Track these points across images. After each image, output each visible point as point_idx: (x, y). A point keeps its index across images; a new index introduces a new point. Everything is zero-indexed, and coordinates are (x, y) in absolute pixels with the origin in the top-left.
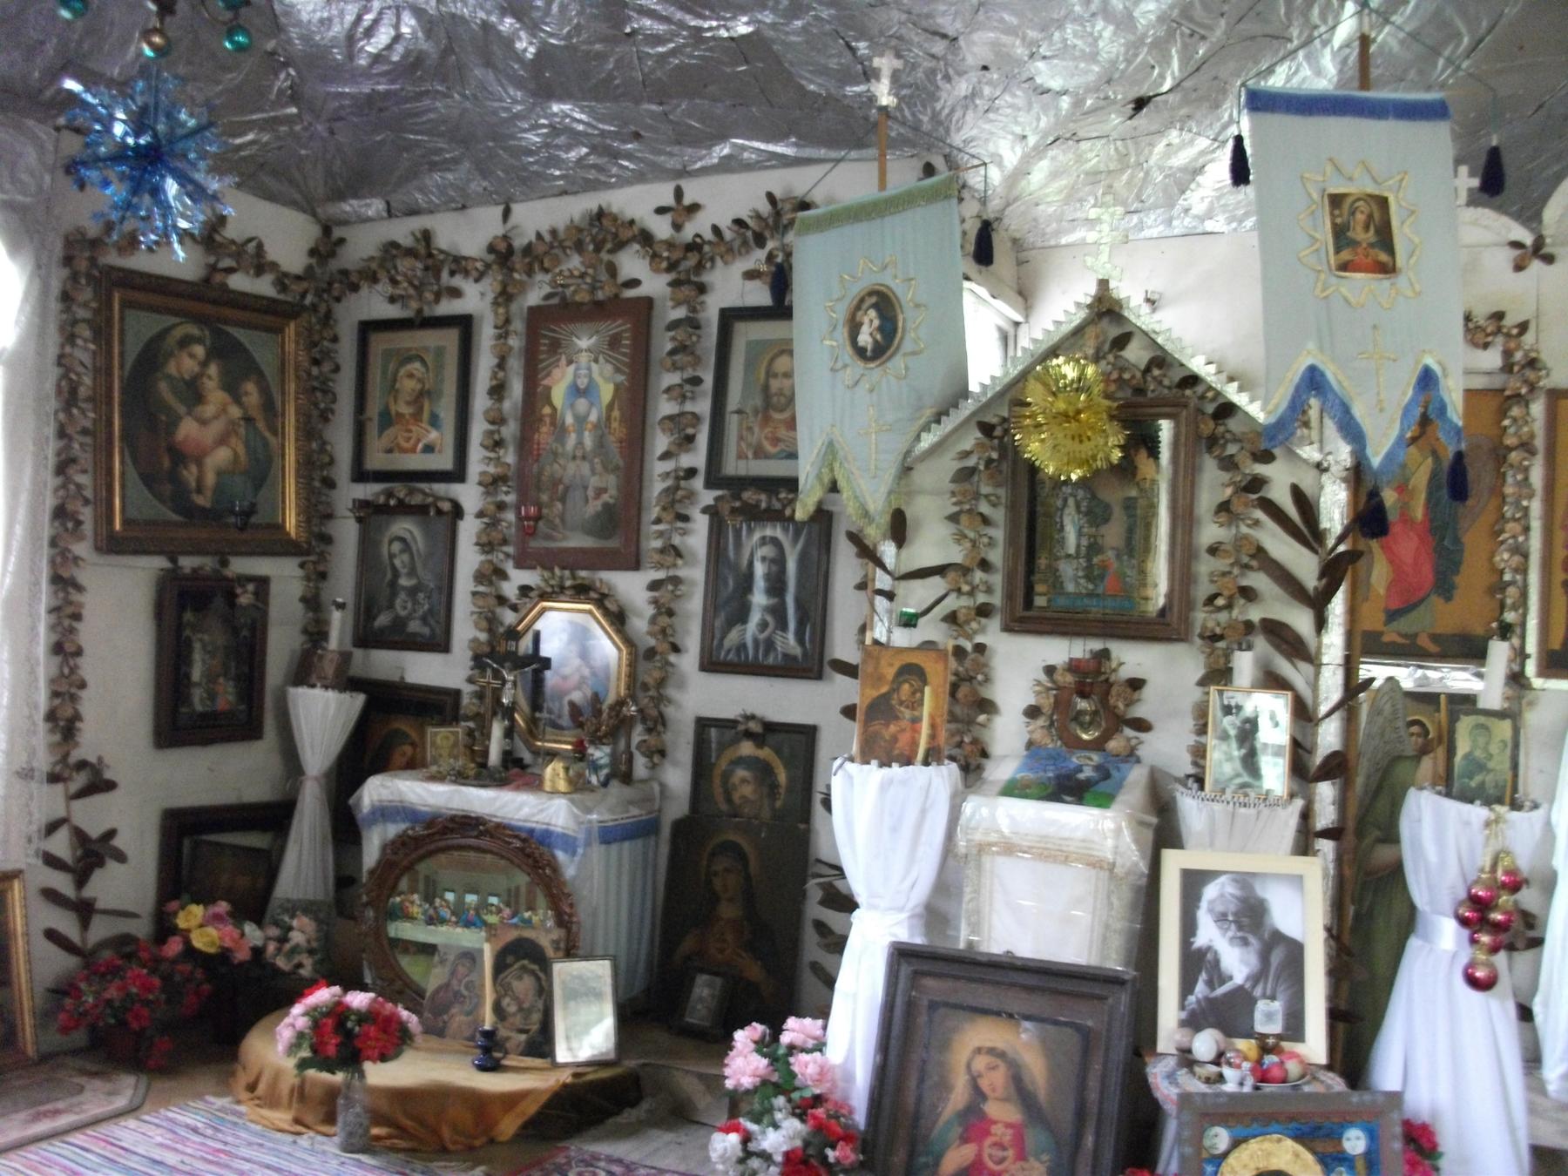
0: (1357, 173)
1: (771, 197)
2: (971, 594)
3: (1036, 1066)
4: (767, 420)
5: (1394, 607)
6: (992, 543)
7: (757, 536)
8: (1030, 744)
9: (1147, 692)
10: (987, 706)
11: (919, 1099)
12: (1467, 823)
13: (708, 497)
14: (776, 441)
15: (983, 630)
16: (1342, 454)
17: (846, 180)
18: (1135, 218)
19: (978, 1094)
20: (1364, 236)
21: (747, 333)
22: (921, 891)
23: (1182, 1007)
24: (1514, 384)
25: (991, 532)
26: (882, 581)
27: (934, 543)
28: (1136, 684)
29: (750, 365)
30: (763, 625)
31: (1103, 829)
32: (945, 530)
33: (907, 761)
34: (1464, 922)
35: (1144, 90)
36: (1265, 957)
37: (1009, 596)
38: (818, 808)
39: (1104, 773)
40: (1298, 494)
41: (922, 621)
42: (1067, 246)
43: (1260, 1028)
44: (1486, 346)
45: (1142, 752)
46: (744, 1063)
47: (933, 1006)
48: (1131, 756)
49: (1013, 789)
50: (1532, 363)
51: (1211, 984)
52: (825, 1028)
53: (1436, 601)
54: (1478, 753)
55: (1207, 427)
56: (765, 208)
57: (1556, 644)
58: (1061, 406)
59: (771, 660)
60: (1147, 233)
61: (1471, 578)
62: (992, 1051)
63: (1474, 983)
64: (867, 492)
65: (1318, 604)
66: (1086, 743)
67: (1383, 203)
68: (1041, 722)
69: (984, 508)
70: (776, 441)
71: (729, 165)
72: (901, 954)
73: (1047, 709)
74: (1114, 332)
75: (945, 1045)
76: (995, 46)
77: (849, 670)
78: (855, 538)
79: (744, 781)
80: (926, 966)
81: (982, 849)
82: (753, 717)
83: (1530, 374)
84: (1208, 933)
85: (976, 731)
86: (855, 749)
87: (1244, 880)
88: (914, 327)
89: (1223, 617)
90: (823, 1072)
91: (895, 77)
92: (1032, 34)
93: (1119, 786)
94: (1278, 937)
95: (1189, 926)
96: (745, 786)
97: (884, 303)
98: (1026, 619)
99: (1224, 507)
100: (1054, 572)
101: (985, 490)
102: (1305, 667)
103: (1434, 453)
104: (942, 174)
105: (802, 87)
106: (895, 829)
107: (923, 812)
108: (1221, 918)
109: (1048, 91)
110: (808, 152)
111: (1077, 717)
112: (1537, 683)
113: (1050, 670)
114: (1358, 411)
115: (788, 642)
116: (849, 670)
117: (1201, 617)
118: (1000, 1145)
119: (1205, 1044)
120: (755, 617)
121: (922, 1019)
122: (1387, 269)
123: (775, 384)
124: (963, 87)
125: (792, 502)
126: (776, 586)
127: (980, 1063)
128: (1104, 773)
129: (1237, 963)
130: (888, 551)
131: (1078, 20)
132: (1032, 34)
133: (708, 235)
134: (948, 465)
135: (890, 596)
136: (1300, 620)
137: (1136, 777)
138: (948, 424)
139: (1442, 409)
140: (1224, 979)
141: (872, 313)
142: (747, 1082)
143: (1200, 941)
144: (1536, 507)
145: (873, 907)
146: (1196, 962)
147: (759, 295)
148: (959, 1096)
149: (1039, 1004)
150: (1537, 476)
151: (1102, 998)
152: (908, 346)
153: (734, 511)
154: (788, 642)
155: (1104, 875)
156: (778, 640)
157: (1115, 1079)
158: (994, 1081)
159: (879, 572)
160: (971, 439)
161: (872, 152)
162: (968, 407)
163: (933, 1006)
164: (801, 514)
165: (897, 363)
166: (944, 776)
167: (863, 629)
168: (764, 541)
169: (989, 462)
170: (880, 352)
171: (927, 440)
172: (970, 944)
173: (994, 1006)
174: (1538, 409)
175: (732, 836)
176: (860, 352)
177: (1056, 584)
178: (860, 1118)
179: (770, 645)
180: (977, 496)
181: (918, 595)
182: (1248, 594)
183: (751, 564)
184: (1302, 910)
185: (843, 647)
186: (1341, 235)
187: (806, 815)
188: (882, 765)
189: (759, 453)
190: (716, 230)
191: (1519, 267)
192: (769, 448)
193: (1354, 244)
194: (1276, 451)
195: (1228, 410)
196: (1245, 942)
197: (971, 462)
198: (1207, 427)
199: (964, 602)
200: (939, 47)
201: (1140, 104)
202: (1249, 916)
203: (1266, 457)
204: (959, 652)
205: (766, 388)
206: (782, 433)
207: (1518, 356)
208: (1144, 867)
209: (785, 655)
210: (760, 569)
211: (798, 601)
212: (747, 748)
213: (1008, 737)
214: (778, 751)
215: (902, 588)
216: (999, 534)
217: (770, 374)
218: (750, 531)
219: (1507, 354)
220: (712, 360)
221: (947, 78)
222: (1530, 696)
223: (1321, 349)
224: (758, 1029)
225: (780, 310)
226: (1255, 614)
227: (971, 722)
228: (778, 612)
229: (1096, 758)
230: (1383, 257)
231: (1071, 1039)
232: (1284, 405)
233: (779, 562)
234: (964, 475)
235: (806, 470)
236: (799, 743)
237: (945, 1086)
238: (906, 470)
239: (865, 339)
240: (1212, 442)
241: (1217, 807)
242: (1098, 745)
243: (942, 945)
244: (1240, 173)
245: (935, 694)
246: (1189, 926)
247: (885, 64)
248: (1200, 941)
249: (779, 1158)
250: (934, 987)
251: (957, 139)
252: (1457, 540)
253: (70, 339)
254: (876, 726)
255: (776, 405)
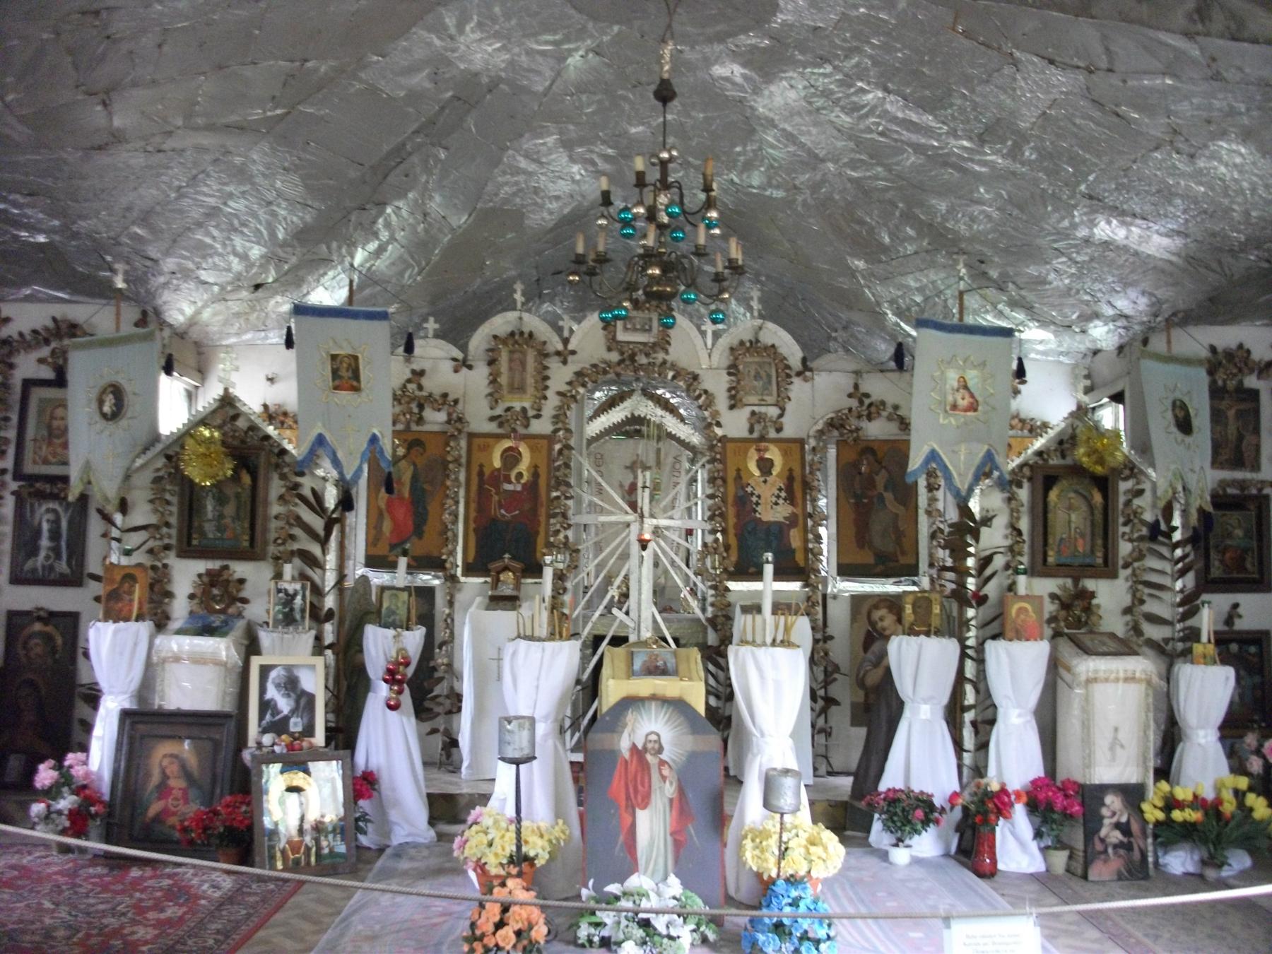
0: (345, 344)
1: (54, 319)
2: (161, 539)
3: (192, 761)
4: (50, 444)
5: (395, 541)
6: (171, 514)
7: (44, 508)
8: (191, 613)
9: (248, 586)
10: (170, 595)
11: (136, 781)
12: (386, 638)
13: (14, 486)
14: (55, 454)
15: (167, 557)
16: (334, 474)
17: (96, 316)
18: (263, 334)
19: (165, 777)
20: (346, 374)
21: (37, 394)
22: (135, 684)
23: (260, 726)
24: (451, 430)
25: (170, 508)
26: (115, 533)
27: (142, 514)
28: (242, 581)
29: (41, 412)
30: (47, 557)
31: (222, 648)
32: (148, 507)
33: (127, 619)
34: (386, 681)
35: (259, 281)
36: (297, 702)
37: (179, 540)
38: (81, 659)
39: (226, 623)
40: (313, 490)
41: (135, 554)
42: (227, 346)
43: (292, 729)
44: (439, 410)
45: (245, 614)
46: (45, 775)
47: (142, 737)
48: (240, 615)
49: (180, 632)
50: (460, 420)
51: (273, 715)
52: (88, 757)
53: (414, 539)
54: (393, 607)
55: (274, 460)
56: (50, 324)
57: (470, 560)
58: (202, 450)
59: (52, 576)
60: (269, 341)
61: (431, 528)
62: (172, 756)
63: (391, 708)
64: (107, 487)
65: (324, 542)
66: (218, 607)
67: (356, 358)
68: (196, 601)
69: (168, 497)
70: (55, 454)
71: (27, 299)
72: (125, 715)
73: (199, 595)
74: (232, 412)
75: (148, 757)
76: (179, 264)
77: (96, 578)
78: (100, 511)
79: (37, 644)
80: (136, 719)
81: (164, 661)
82: (41, 609)
83: (458, 425)
84: (272, 693)
85: (165, 607)
86: (101, 616)
87: (289, 668)
88: (133, 405)
89: (281, 548)
90: (88, 774)
91: (126, 273)
92: (197, 260)
93: (231, 629)
94: (304, 693)
95: (263, 690)
96: (37, 647)
97: (117, 391)
98: (188, 551)
99: (281, 498)
100: (201, 527)
101: (168, 487)
102: (318, 571)
103: (415, 465)
104: (149, 317)
105: (74, 269)
106: (121, 654)
107: (136, 644)
108: (278, 686)
109: (206, 283)
110: (74, 298)
111: (213, 598)
112: (463, 579)
113: (200, 576)
114: (340, 455)
115: (63, 567)
116: (96, 578)
117: (272, 549)
118: (176, 799)
119: (267, 739)
120: (43, 554)
121: (137, 744)
122: (356, 389)
123: (55, 423)
124: (162, 279)
125: (64, 489)
126: (55, 535)
127: (165, 763)
128: (226, 623)
129: (284, 705)
130: (118, 518)
131: (220, 255)
132: (197, 260)
133: (16, 336)
134: (148, 475)
135: (118, 540)
136: (316, 549)
137: (240, 625)
138: (150, 454)
139: (382, 452)
140: (279, 712)
141: (111, 396)
142: (47, 783)
143: (268, 696)
144: (462, 493)
145: (111, 693)
146: (265, 706)
147: (47, 373)
148: (156, 779)
149: (195, 731)
150: (462, 477)
151: (221, 725)
152: (129, 414)
153: (30, 494)
154: (63, 567)
155: (223, 669)
156: (56, 565)
157: (229, 764)
158: (173, 769)
159: (114, 529)
160: (161, 462)
161: (113, 302)
162: (159, 447)
163: (142, 737)
164: (71, 498)
165: (124, 423)
166: (145, 628)
167: (105, 558)
168: (48, 511)
169: (170, 474)
170: (115, 416)
171: (139, 462)
172: (160, 706)
173: (169, 733)
174: (463, 443)
175: (30, 676)
176: (104, 416)
177: (203, 534)
178: (107, 797)
179: (51, 568)
180: (164, 490)
181: (134, 540)
182: (292, 537)
183: (40, 524)
184: (314, 681)
185: (93, 566)
186: (335, 373)
187: (73, 660)
188: (115, 622)
189: (46, 462)
190: (21, 334)
191: (456, 371)
192: (50, 458)
193: (341, 377)
194: (306, 471)
195: (284, 452)
196: (288, 696)
197: (160, 474)
198: (274, 460)
199: (158, 543)
200: (148, 263)
201: (257, 287)
202: (291, 684)
203: (302, 474)
204: (154, 568)
205: (49, 427)
206: (59, 450)
207: (455, 416)
208: (240, 663)
209: (61, 574)
210: (45, 526)
211: (68, 546)
212: (38, 627)
213: (180, 608)
214: (56, 627)
215: (126, 537)
216: (174, 509)
217: (52, 418)
218: (40, 505)
219: (449, 415)
220: (17, 407)
221: (153, 275)
222: (458, 586)
223: (324, 426)
224: (51, 762)
225: (60, 381)
226: (296, 546)
227: (161, 603)
228: (56, 551)
229: (222, 617)
230: (355, 383)
231: (208, 746)
232: (306, 451)
233: (56, 523)
234: (157, 480)
235: (74, 472)
236: (70, 624)
237: (148, 775)
238: (127, 477)
239: (107, 409)
240: (277, 466)
241: (275, 635)
242: (223, 611)
243: (147, 709)
244: (289, 343)
245: (141, 589)
246: (263, 690)
247: (120, 267)
248: (268, 696)
249: (66, 812)
250: (142, 728)
251: (159, 302)
252: (425, 508)
253: (450, 665)
254: (112, 604)
255: (57, 435)
